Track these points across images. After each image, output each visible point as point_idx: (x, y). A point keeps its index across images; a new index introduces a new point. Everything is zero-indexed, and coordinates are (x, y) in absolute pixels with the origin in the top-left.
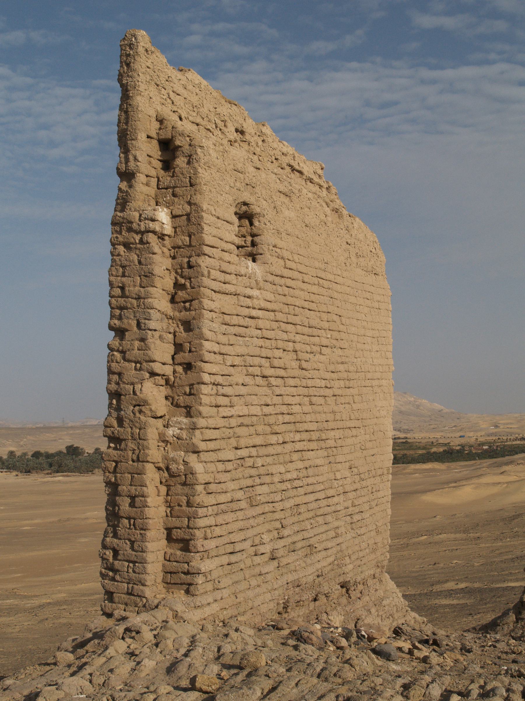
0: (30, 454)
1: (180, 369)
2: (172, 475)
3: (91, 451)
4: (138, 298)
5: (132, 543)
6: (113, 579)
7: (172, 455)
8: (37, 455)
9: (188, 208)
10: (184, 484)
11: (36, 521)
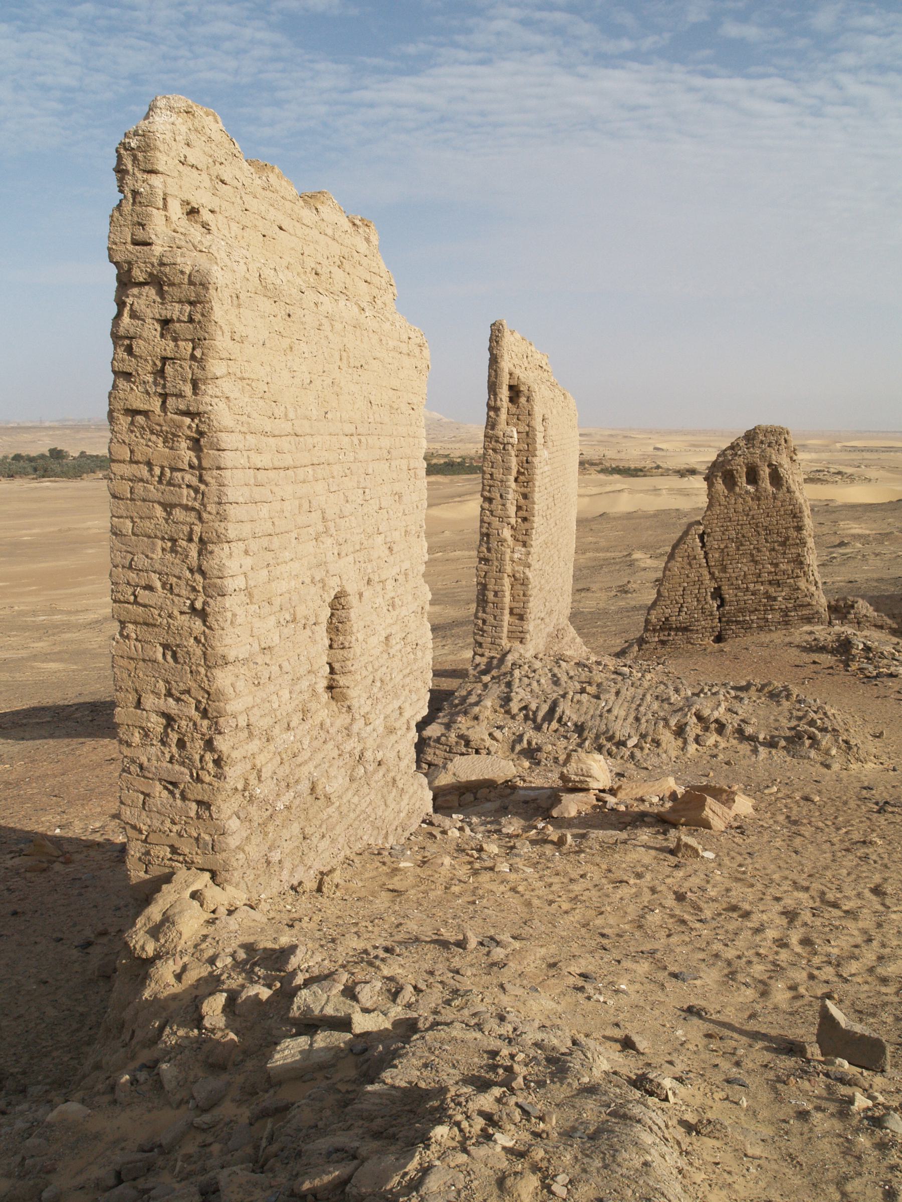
0: (11, 456)
1: (519, 520)
2: (516, 579)
3: (76, 455)
4: (502, 481)
5: (495, 617)
6: (482, 636)
7: (516, 569)
8: (17, 458)
9: (527, 429)
10: (522, 584)
11: (34, 531)
